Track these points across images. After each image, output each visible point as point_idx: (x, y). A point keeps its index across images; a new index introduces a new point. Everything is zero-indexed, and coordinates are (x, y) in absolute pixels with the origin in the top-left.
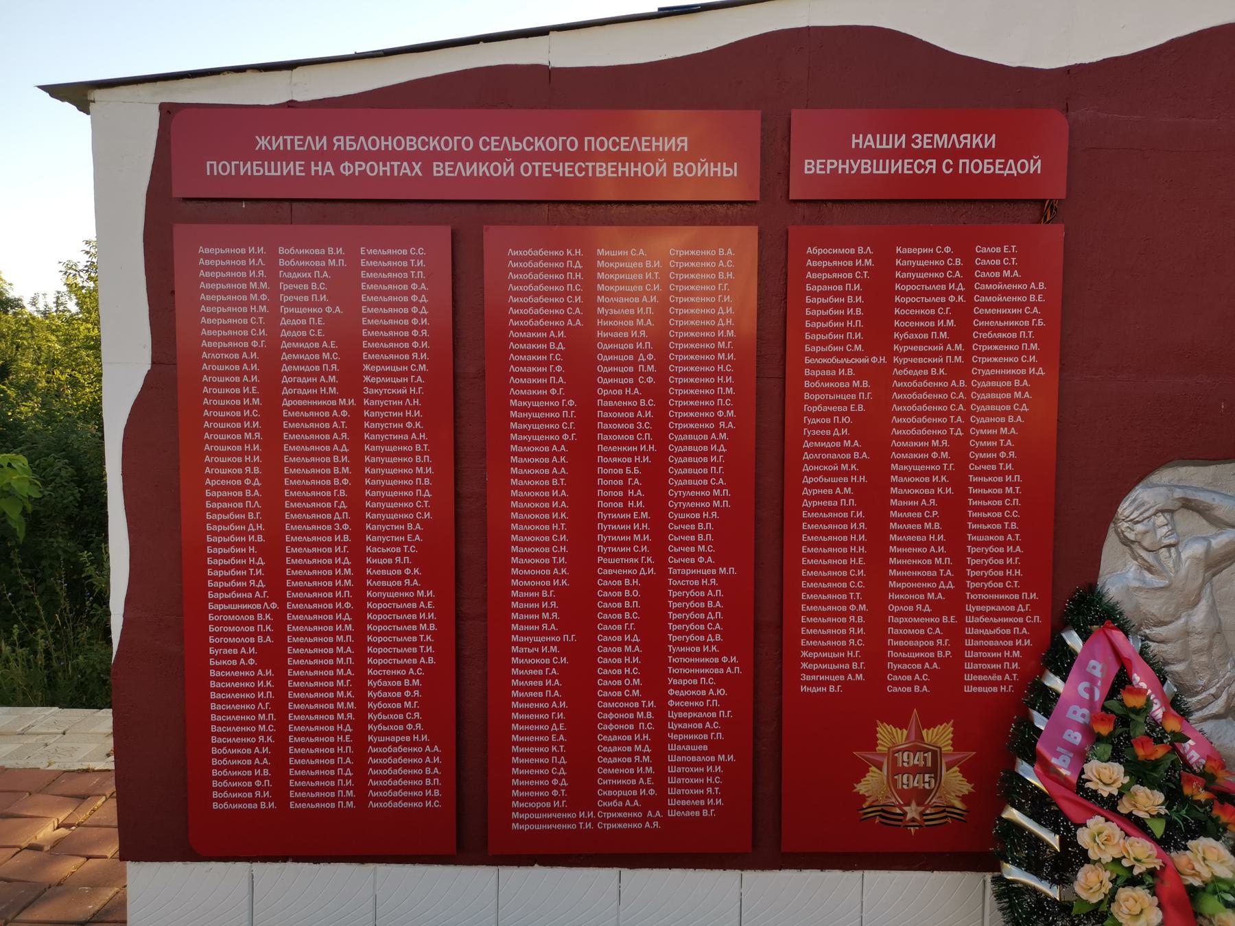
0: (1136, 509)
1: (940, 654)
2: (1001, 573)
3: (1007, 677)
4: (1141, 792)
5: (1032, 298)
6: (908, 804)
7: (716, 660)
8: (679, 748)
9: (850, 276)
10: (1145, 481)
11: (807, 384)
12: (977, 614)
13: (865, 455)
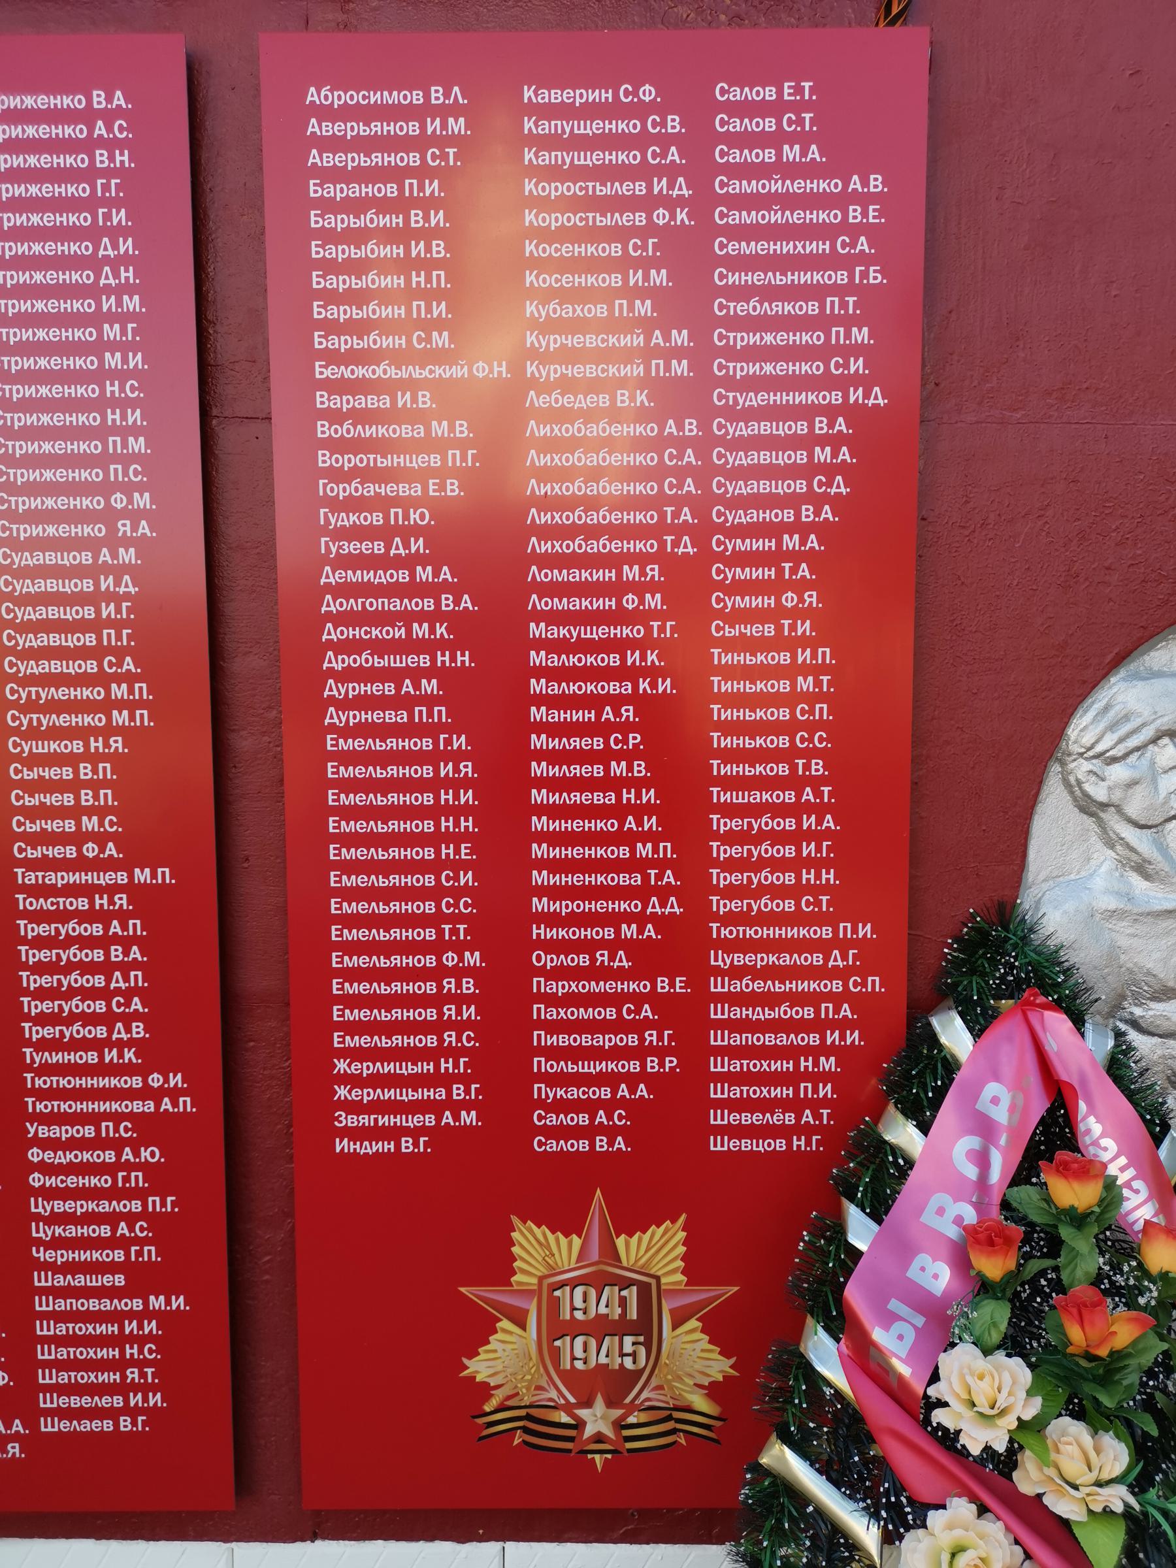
0: (1112, 728)
1: (652, 1064)
2: (789, 878)
3: (808, 1116)
4: (1070, 1434)
5: (855, 214)
6: (588, 1403)
7: (136, 1082)
8: (60, 1281)
9: (414, 159)
10: (1132, 666)
11: (323, 430)
12: (736, 973)
13: (466, 602)
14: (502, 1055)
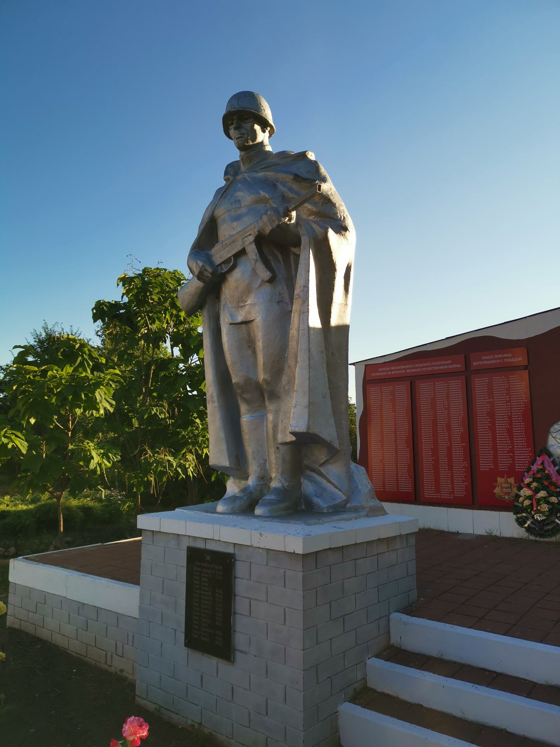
14: (495, 462)
